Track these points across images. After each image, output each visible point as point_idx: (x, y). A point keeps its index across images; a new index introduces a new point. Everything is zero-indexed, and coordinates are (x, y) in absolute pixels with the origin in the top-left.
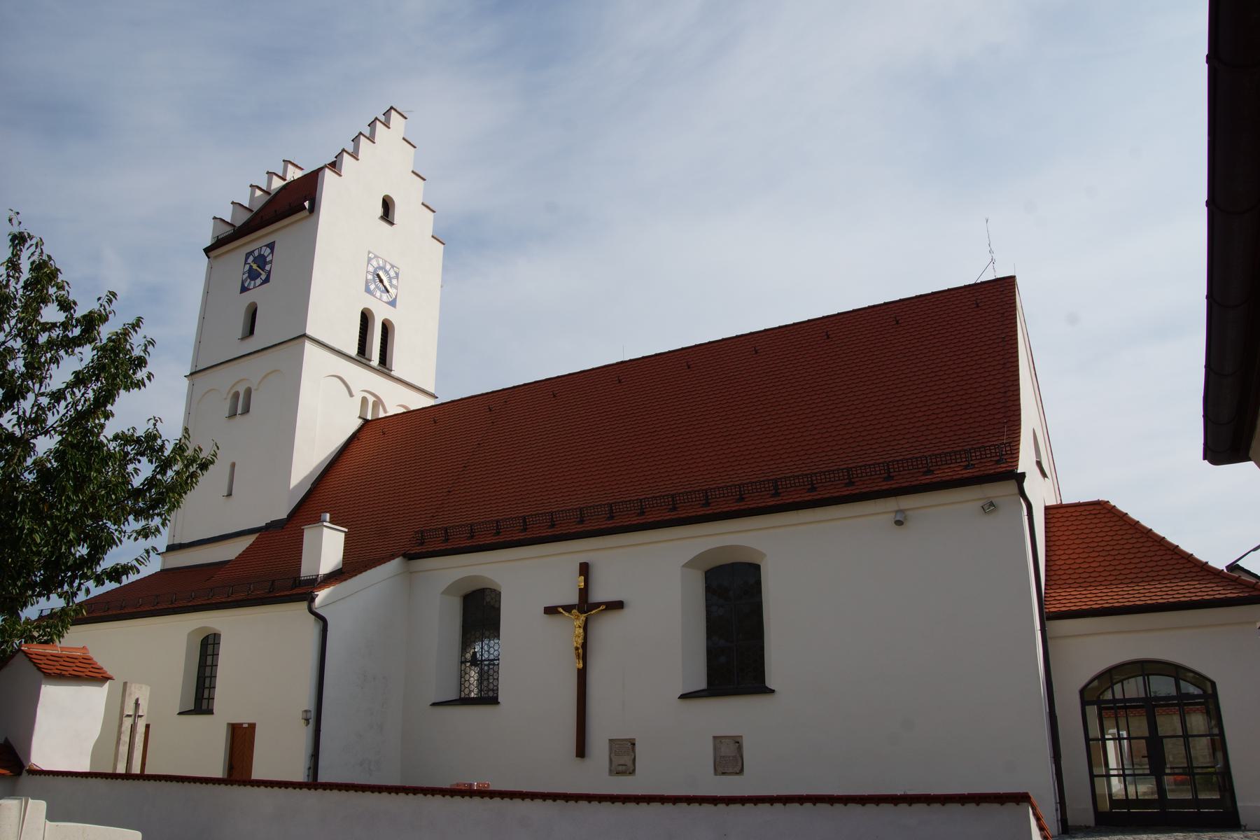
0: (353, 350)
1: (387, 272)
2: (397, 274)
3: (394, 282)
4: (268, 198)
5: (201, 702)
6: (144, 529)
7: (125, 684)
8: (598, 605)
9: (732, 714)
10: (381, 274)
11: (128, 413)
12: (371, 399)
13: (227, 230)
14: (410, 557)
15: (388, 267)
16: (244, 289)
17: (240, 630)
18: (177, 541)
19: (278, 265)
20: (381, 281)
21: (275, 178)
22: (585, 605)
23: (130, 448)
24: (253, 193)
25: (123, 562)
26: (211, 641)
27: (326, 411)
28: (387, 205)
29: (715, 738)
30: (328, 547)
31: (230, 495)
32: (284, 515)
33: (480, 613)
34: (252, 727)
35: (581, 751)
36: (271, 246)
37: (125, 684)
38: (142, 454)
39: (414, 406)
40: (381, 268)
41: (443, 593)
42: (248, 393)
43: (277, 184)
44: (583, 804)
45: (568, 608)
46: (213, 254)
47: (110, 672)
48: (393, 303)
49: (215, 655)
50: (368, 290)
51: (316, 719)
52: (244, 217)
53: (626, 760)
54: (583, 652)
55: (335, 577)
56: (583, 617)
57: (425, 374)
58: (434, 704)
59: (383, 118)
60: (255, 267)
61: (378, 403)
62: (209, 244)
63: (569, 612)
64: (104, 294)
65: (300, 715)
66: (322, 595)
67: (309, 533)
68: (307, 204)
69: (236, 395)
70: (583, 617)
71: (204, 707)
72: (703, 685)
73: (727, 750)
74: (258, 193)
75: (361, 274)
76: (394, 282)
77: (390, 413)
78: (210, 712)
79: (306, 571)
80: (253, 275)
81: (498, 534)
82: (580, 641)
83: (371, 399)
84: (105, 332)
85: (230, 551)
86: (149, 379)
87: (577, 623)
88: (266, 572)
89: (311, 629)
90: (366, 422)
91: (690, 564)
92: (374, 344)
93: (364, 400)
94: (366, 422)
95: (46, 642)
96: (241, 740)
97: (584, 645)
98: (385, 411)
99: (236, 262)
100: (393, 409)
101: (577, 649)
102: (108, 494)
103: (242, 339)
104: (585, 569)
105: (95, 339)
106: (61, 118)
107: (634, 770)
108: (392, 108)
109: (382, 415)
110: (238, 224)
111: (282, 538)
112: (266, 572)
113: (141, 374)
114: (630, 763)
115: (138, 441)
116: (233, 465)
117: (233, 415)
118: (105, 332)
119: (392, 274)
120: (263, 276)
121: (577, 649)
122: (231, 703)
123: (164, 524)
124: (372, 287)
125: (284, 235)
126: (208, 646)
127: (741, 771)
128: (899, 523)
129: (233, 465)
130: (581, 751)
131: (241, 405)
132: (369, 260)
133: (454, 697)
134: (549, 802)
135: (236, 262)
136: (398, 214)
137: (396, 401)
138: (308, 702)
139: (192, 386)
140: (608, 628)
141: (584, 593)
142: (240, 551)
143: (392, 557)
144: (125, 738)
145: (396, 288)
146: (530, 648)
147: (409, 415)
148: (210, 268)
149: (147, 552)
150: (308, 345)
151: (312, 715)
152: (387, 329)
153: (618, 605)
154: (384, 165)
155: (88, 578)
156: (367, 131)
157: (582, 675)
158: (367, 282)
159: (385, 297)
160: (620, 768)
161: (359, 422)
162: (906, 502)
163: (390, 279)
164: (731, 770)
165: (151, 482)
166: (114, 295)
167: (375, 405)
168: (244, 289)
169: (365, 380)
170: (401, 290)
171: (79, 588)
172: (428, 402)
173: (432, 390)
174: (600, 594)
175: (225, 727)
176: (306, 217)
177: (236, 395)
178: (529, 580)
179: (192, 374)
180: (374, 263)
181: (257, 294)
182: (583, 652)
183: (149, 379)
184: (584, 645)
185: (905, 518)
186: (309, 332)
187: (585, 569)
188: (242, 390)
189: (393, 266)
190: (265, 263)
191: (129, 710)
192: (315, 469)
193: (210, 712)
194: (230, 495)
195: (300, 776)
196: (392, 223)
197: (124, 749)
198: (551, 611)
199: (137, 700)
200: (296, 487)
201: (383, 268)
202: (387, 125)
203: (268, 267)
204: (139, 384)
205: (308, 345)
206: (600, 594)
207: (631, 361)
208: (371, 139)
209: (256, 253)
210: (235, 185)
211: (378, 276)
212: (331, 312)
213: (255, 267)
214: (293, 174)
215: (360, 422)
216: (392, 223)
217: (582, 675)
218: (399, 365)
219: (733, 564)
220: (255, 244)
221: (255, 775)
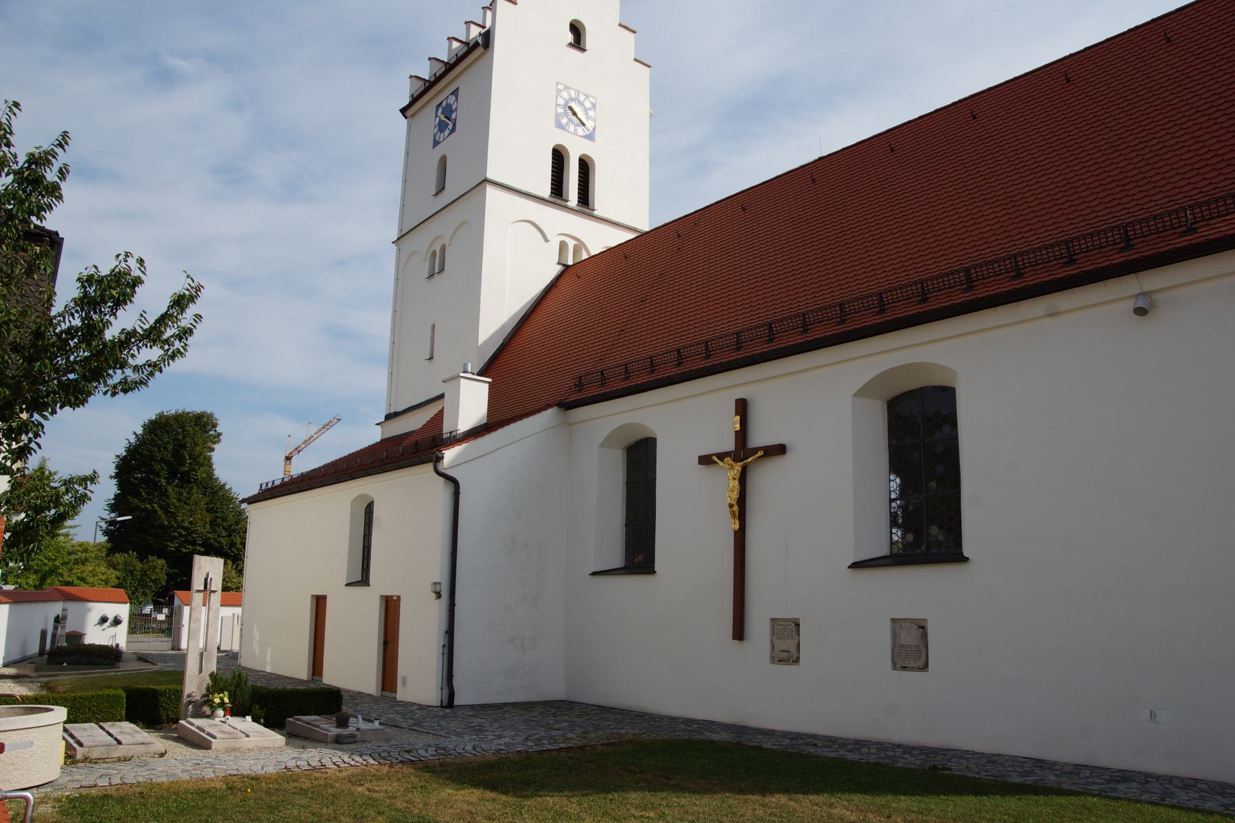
0: (545, 190)
1: (581, 104)
2: (594, 106)
3: (591, 113)
8: (756, 450)
9: (918, 589)
12: (571, 243)
14: (567, 406)
15: (582, 98)
16: (436, 143)
19: (461, 116)
20: (575, 114)
21: (472, 26)
27: (518, 257)
28: (577, 30)
29: (894, 620)
35: (739, 633)
36: (455, 93)
40: (572, 99)
41: (603, 445)
42: (443, 248)
45: (722, 456)
46: (409, 113)
48: (590, 137)
51: (449, 593)
53: (789, 645)
55: (475, 433)
58: (594, 574)
60: (443, 118)
61: (580, 246)
62: (406, 102)
65: (428, 589)
69: (434, 253)
70: (738, 467)
72: (617, 561)
73: (909, 638)
74: (456, 45)
76: (591, 113)
79: (447, 428)
80: (442, 127)
82: (735, 495)
83: (571, 243)
87: (731, 474)
89: (442, 491)
91: (863, 392)
92: (570, 181)
93: (563, 246)
97: (742, 500)
99: (429, 117)
101: (731, 506)
104: (742, 407)
107: (798, 659)
109: (585, 256)
114: (793, 649)
115: (100, 281)
116: (433, 327)
117: (431, 276)
119: (588, 105)
120: (450, 127)
124: (564, 121)
125: (465, 81)
127: (925, 667)
128: (1140, 312)
129: (433, 327)
130: (739, 633)
131: (437, 265)
132: (559, 91)
133: (884, 550)
135: (429, 117)
136: (589, 40)
138: (439, 573)
140: (767, 477)
141: (742, 436)
143: (548, 406)
146: (690, 506)
148: (409, 128)
150: (490, 191)
152: (585, 167)
153: (779, 450)
159: (580, 130)
160: (783, 655)
162: (1152, 280)
163: (586, 110)
164: (912, 664)
166: (16, 105)
167: (577, 250)
168: (436, 143)
174: (760, 437)
176: (481, 56)
177: (434, 253)
178: (682, 423)
184: (742, 500)
185: (1153, 305)
186: (490, 176)
187: (742, 407)
188: (438, 248)
189: (587, 97)
190: (452, 112)
192: (511, 319)
194: (431, 358)
196: (583, 50)
198: (705, 460)
200: (485, 343)
205: (490, 191)
206: (760, 437)
211: (570, 108)
212: (515, 145)
216: (583, 50)
219: (921, 388)
220: (442, 94)
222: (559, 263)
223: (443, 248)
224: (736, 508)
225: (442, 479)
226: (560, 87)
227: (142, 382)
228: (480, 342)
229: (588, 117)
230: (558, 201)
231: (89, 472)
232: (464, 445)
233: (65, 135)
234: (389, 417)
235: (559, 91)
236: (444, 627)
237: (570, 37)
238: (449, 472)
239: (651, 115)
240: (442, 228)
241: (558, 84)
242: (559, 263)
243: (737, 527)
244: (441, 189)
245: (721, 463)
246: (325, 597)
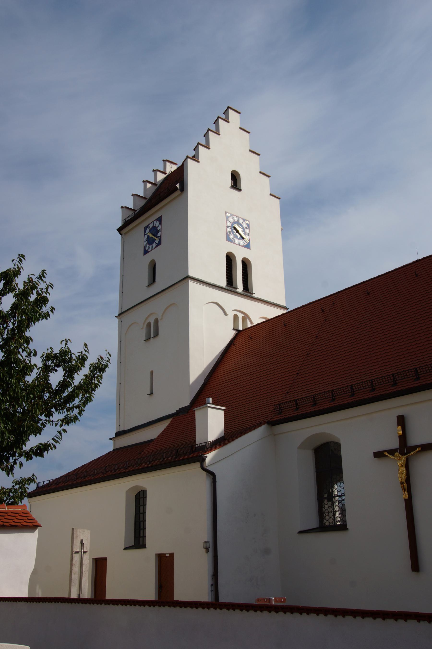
0: (223, 283)
1: (241, 225)
2: (248, 226)
3: (247, 231)
4: (155, 188)
5: (138, 540)
6: (66, 418)
7: (73, 529)
10: (237, 226)
11: (43, 337)
12: (240, 316)
13: (130, 214)
14: (272, 423)
15: (241, 221)
16: (146, 252)
17: (160, 486)
18: (121, 429)
19: (166, 233)
20: (237, 232)
21: (158, 173)
22: (405, 449)
23: (50, 362)
24: (145, 186)
25: (44, 441)
26: (141, 496)
27: (209, 328)
28: (235, 177)
30: (213, 421)
31: (152, 393)
32: (188, 404)
33: (327, 462)
34: (172, 555)
36: (159, 219)
37: (73, 529)
38: (58, 366)
39: (270, 317)
40: (236, 223)
42: (156, 322)
43: (161, 177)
44: (349, 618)
45: (392, 452)
46: (123, 232)
47: (39, 522)
48: (248, 246)
49: (145, 505)
50: (229, 240)
51: (213, 547)
52: (142, 203)
54: (408, 485)
55: (219, 442)
56: (404, 458)
57: (275, 292)
58: (301, 532)
59: (223, 116)
60: (151, 235)
61: (246, 317)
62: (120, 225)
63: (393, 455)
64: (16, 257)
65: (202, 545)
66: (210, 457)
67: (198, 413)
68: (178, 186)
69: (149, 325)
70: (404, 458)
71: (141, 543)
72: (315, 524)
74: (149, 185)
75: (222, 230)
76: (247, 231)
77: (255, 324)
78: (143, 546)
79: (199, 440)
80: (150, 241)
81: (334, 400)
82: (404, 476)
83: (240, 316)
84: (20, 282)
85: (153, 433)
86: (52, 311)
87: (400, 463)
88: (173, 445)
90: (239, 332)
92: (238, 276)
93: (236, 317)
94: (239, 332)
95: (12, 504)
96: (165, 565)
97: (408, 480)
98: (251, 323)
99: (139, 235)
100: (256, 320)
101: (402, 483)
102: (28, 394)
103: (149, 286)
105: (14, 289)
106: (38, 168)
108: (229, 107)
109: (249, 325)
110: (138, 208)
111: (184, 419)
112: (173, 445)
113: (45, 310)
115: (55, 357)
116: (152, 373)
117: (148, 339)
118: (20, 282)
119: (245, 225)
120: (157, 241)
121: (402, 483)
122: (158, 539)
123: (80, 413)
124: (232, 237)
125: (166, 211)
126: (140, 499)
129: (152, 373)
131: (152, 331)
132: (227, 218)
134: (321, 616)
135: (139, 235)
136: (244, 183)
137: (258, 314)
138: (205, 535)
139: (121, 322)
141: (403, 439)
142: (161, 432)
144: (76, 568)
145: (249, 235)
147: (268, 322)
148: (123, 241)
149: (60, 433)
150: (191, 284)
151: (211, 545)
152: (246, 265)
154: (229, 148)
155: (20, 455)
156: (213, 128)
157: (409, 504)
158: (227, 233)
159: (242, 242)
161: (234, 333)
163: (244, 229)
165: (63, 385)
166: (23, 256)
168: (146, 252)
169: (234, 303)
170: (254, 235)
171: (15, 463)
172: (280, 312)
173: (283, 304)
174: (416, 438)
175: (154, 555)
177: (149, 325)
179: (120, 315)
180: (231, 220)
181: (155, 254)
182: (408, 485)
183: (52, 311)
184: (408, 480)
186: (191, 274)
187: (401, 421)
189: (244, 220)
190: (157, 232)
191: (77, 548)
193: (143, 546)
194: (152, 393)
195: (205, 596)
196: (240, 190)
197: (75, 577)
198: (379, 455)
199: (82, 541)
200: (194, 383)
201: (237, 222)
202: (227, 120)
203: (159, 235)
204: (46, 316)
205: (191, 284)
206: (416, 438)
207: (424, 258)
208: (217, 132)
209: (151, 226)
210: (132, 185)
211: (235, 228)
212: (205, 258)
213: (151, 235)
214: (171, 168)
215: (234, 332)
216: (240, 190)
217: (409, 504)
218: (258, 290)
220: (149, 219)
221: (109, 596)
222: (234, 329)
223: (156, 322)
224: (405, 485)
225: (205, 473)
226: (227, 214)
227: (76, 418)
228: (191, 382)
229: (245, 234)
230: (232, 289)
231: (30, 476)
232: (217, 451)
233: (44, 272)
234: (119, 434)
235: (227, 218)
236: (211, 572)
237: (230, 182)
238: (209, 468)
239: (282, 230)
240: (155, 308)
241: (226, 213)
242: (234, 329)
243: (407, 496)
244: (153, 279)
245: (391, 457)
246: (104, 560)
